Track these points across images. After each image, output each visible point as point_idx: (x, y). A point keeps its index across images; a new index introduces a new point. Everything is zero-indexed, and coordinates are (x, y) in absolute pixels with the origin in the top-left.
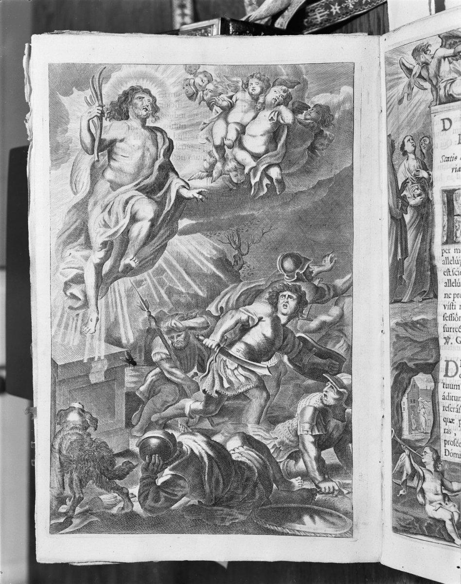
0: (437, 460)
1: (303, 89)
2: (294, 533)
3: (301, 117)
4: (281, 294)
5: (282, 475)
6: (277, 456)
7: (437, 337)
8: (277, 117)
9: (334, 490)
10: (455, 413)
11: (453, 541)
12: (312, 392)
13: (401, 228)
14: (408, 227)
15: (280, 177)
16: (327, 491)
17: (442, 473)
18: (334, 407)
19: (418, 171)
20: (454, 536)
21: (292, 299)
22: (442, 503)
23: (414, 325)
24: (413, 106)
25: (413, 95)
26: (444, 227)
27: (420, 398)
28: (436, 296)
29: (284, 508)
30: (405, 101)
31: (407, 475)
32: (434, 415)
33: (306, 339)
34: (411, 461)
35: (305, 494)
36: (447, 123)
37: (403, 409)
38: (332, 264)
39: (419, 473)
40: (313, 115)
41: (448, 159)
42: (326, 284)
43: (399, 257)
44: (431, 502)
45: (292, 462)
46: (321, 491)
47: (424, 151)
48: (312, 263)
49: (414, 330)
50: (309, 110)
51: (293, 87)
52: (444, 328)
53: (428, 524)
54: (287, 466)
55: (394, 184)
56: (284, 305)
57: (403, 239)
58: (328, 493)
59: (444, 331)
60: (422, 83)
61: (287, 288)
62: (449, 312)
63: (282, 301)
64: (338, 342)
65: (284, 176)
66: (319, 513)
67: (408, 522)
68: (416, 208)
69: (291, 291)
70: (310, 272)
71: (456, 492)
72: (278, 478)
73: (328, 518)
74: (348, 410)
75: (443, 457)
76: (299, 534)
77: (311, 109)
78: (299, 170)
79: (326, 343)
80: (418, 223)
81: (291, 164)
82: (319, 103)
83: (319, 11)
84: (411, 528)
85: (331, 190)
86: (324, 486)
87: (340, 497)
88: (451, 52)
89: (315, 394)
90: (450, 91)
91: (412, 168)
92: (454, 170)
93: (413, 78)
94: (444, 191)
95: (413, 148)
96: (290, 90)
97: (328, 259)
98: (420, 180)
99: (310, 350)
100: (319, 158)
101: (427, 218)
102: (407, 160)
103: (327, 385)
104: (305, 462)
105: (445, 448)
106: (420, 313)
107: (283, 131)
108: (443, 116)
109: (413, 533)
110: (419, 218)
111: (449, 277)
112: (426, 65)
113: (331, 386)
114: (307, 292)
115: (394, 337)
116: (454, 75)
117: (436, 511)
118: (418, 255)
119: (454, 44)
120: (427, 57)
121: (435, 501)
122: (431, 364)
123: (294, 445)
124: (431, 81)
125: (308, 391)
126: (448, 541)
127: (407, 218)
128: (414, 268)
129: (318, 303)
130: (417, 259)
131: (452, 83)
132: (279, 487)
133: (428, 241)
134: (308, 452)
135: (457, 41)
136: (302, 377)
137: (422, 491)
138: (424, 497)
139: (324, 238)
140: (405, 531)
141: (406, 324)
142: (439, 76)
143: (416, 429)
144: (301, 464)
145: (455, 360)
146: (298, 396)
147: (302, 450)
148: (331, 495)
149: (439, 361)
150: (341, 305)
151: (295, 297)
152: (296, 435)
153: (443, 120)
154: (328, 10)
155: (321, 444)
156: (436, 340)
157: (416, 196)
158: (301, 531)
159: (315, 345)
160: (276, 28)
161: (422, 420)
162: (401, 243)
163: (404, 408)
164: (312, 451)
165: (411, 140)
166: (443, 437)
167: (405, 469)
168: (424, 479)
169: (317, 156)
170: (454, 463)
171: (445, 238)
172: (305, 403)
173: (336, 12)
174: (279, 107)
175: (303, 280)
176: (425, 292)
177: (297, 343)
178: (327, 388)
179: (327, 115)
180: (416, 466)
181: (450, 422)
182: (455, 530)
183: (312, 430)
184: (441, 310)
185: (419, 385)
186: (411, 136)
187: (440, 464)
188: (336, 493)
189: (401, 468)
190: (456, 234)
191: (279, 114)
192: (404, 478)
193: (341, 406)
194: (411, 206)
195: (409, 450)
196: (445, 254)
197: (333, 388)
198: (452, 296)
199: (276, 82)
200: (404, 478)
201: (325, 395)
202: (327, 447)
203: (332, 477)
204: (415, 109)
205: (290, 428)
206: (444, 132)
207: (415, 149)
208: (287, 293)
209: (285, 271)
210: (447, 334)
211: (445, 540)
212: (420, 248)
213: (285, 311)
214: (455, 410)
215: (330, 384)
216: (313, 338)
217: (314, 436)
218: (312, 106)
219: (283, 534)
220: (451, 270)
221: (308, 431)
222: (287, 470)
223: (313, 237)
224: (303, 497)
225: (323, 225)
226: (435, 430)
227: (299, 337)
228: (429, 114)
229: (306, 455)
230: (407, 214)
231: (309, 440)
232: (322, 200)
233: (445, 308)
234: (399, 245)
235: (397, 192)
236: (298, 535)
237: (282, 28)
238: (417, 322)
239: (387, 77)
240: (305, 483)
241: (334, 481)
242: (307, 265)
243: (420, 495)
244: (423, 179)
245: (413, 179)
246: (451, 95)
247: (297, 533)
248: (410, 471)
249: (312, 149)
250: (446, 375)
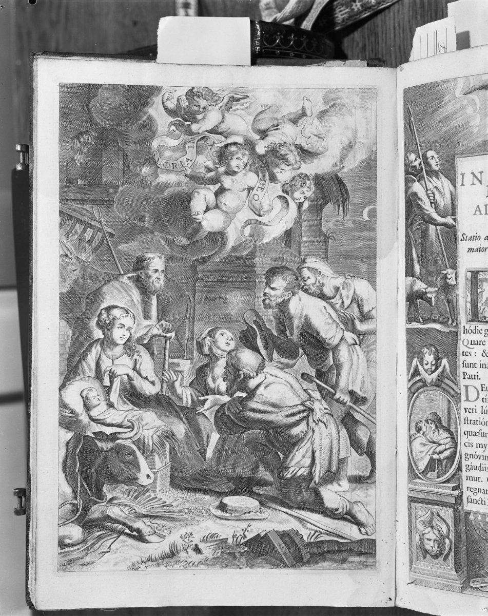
83: (339, 10)
154: (349, 8)
173: (358, 9)
180: (419, 365)
233: (466, 412)
237: (307, 29)
250: (467, 400)
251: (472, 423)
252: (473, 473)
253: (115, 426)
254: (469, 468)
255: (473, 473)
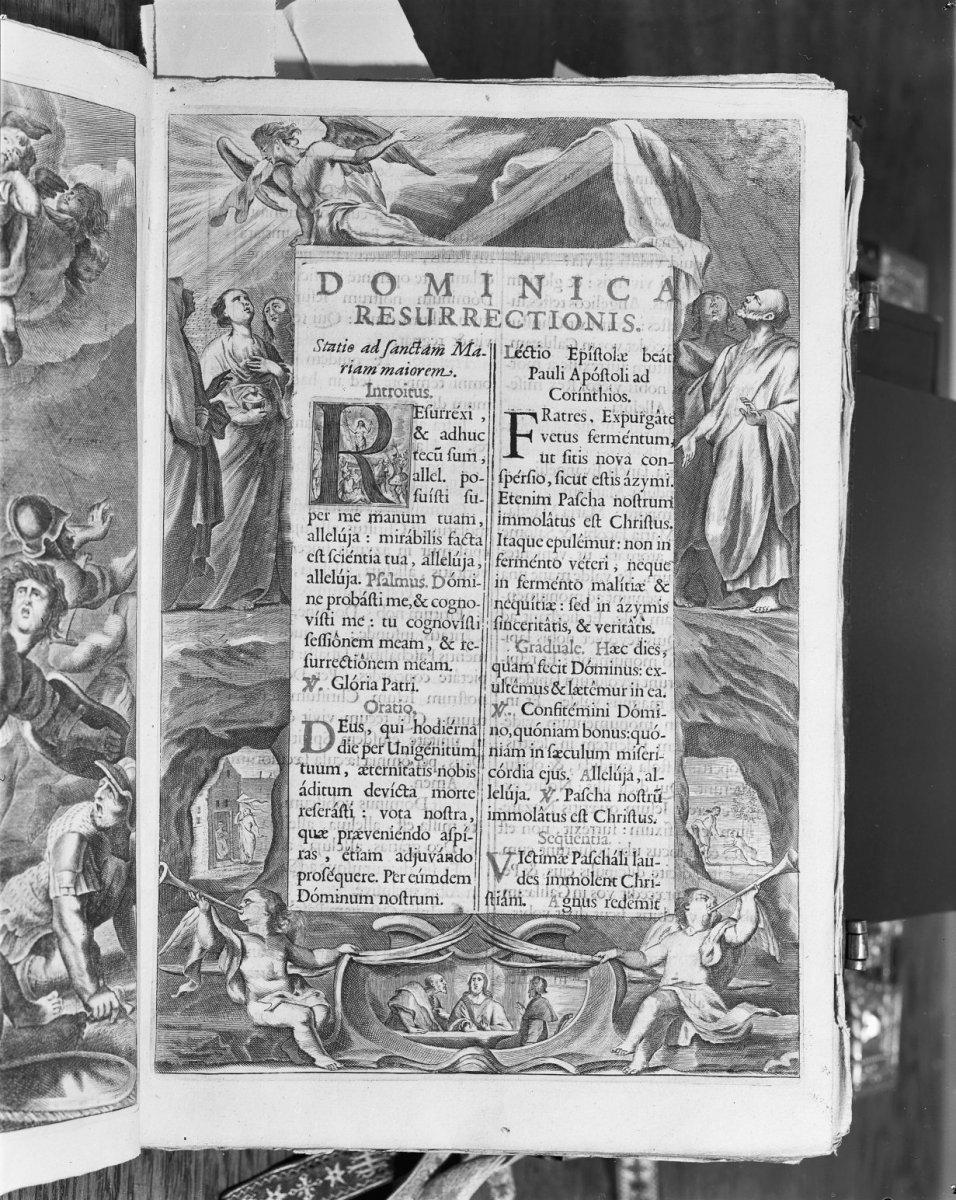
0: (278, 911)
1: (56, 146)
2: (45, 1119)
3: (51, 203)
4: (19, 585)
5: (21, 994)
6: (10, 952)
7: (287, 676)
8: (10, 194)
9: (112, 1009)
10: (330, 819)
11: (312, 1062)
12: (73, 802)
13: (205, 465)
14: (223, 464)
15: (11, 328)
16: (101, 1014)
17: (290, 937)
18: (115, 829)
19: (256, 360)
20: (313, 1052)
21: (39, 597)
22: (287, 994)
23: (230, 655)
24: (248, 235)
25: (251, 213)
26: (313, 472)
27: (244, 797)
28: (287, 600)
29: (25, 1067)
30: (230, 219)
31: (203, 950)
32: (275, 827)
33: (68, 688)
34: (212, 923)
35: (66, 1027)
36: (331, 284)
37: (194, 821)
38: (106, 524)
39: (232, 942)
40: (73, 204)
41: (332, 347)
42: (99, 567)
43: (198, 519)
44: (260, 996)
45: (40, 961)
46: (92, 1016)
47: (272, 325)
48: (70, 520)
49: (229, 664)
50: (66, 192)
51: (38, 137)
52: (306, 660)
53: (252, 1039)
54: (30, 971)
55: (189, 377)
56: (24, 610)
57: (210, 488)
58: (103, 1018)
59: (306, 666)
60: (274, 196)
61: (27, 571)
62: (318, 631)
63: (20, 599)
64: (118, 691)
65: (20, 327)
66: (87, 1065)
67: (200, 1045)
68: (247, 429)
69: (36, 579)
70: (67, 538)
71: (322, 968)
72: (12, 1001)
73: (102, 1072)
74: (132, 835)
75: (293, 904)
76: (54, 1119)
77: (69, 191)
78: (48, 317)
79: (100, 694)
80: (250, 458)
81: (35, 301)
82: (83, 181)
83: (366, 1171)
84: (208, 1055)
85: (104, 370)
86: (99, 1003)
87: (120, 1021)
88: (350, 153)
89: (81, 805)
90: (342, 224)
91: (240, 353)
92: (347, 370)
93: (254, 184)
94: (318, 405)
95: (248, 316)
96: (33, 142)
97: (97, 513)
98: (259, 377)
99: (74, 710)
100: (85, 298)
101: (273, 451)
102: (231, 335)
103: (101, 784)
104: (64, 958)
105: (300, 887)
106: (247, 632)
107: (20, 227)
108: (324, 267)
109: (215, 1065)
110: (253, 448)
111: (320, 566)
112: (285, 164)
113: (109, 787)
114: (66, 581)
115: (176, 677)
116: (353, 197)
117: (272, 1010)
118: (249, 519)
119: (355, 142)
120: (289, 150)
121: (270, 993)
122: (269, 729)
123: (43, 921)
124: (295, 197)
125: (67, 799)
126: (300, 1065)
127: (222, 447)
128: (237, 545)
129: (87, 607)
130: (246, 528)
131: (348, 210)
132: (15, 1020)
133: (276, 495)
134: (68, 935)
135: (365, 137)
136: (56, 770)
137: (241, 978)
138: (244, 988)
139: (92, 469)
140: (191, 1065)
141: (210, 653)
142: (318, 192)
143: (227, 858)
144: (57, 960)
145: (327, 720)
146: (48, 813)
147: (59, 930)
148: (107, 1021)
149: (287, 724)
150: (123, 612)
151: (43, 590)
152: (48, 901)
153: (323, 274)
154: (349, 1172)
155: (92, 915)
156: (284, 685)
157: (249, 406)
158: (57, 1112)
159: (82, 697)
160: (139, 10)
161: (246, 838)
162: (205, 495)
163: (198, 819)
164: (76, 928)
165: (242, 299)
166: (295, 865)
167: (196, 940)
168: (244, 953)
169: (82, 292)
170: (321, 914)
171: (317, 493)
172: (61, 826)
174: (11, 173)
175: (56, 556)
176: (262, 591)
177: (49, 694)
178: (100, 790)
179: (96, 211)
180: (226, 931)
181: (316, 837)
182: (317, 1040)
183: (76, 885)
184: (299, 626)
185: (240, 771)
186: (244, 292)
187: (285, 918)
188: (115, 1015)
189: (184, 938)
190: (343, 486)
191: (12, 189)
192: (194, 956)
193: (125, 826)
194: (235, 424)
195: (209, 900)
196: (316, 523)
197: (111, 790)
198: (325, 601)
199: (8, 120)
200: (194, 956)
201: (99, 807)
202: (103, 919)
203: (109, 982)
204: (254, 241)
205: (35, 886)
206: (323, 296)
207: (251, 319)
208: (30, 583)
209: (22, 534)
210: (310, 672)
211: (292, 1063)
212: (255, 507)
213: (25, 624)
214: (330, 813)
215: (107, 783)
216: (78, 683)
217: (81, 898)
218: (71, 185)
219: (23, 1125)
220: (326, 553)
221: (68, 888)
222: (29, 979)
223: (73, 465)
224: (63, 1036)
225: (92, 441)
226: (277, 855)
227: (54, 682)
228: (291, 257)
229: (65, 941)
230: (223, 438)
231: (70, 906)
232: (88, 387)
233: (545, 440)
234: (198, 499)
235: (196, 393)
236: (52, 1123)
238: (240, 649)
239: (172, 165)
240: (68, 1002)
241: (112, 989)
242: (61, 525)
243: (235, 987)
244: (270, 377)
245: (242, 375)
246: (344, 231)
247: (51, 1118)
248: (209, 942)
249: (72, 274)
250: (307, 748)
251: (458, 817)
252: (653, 471)
253: (717, 883)
254: (653, 422)
255: (653, 471)
